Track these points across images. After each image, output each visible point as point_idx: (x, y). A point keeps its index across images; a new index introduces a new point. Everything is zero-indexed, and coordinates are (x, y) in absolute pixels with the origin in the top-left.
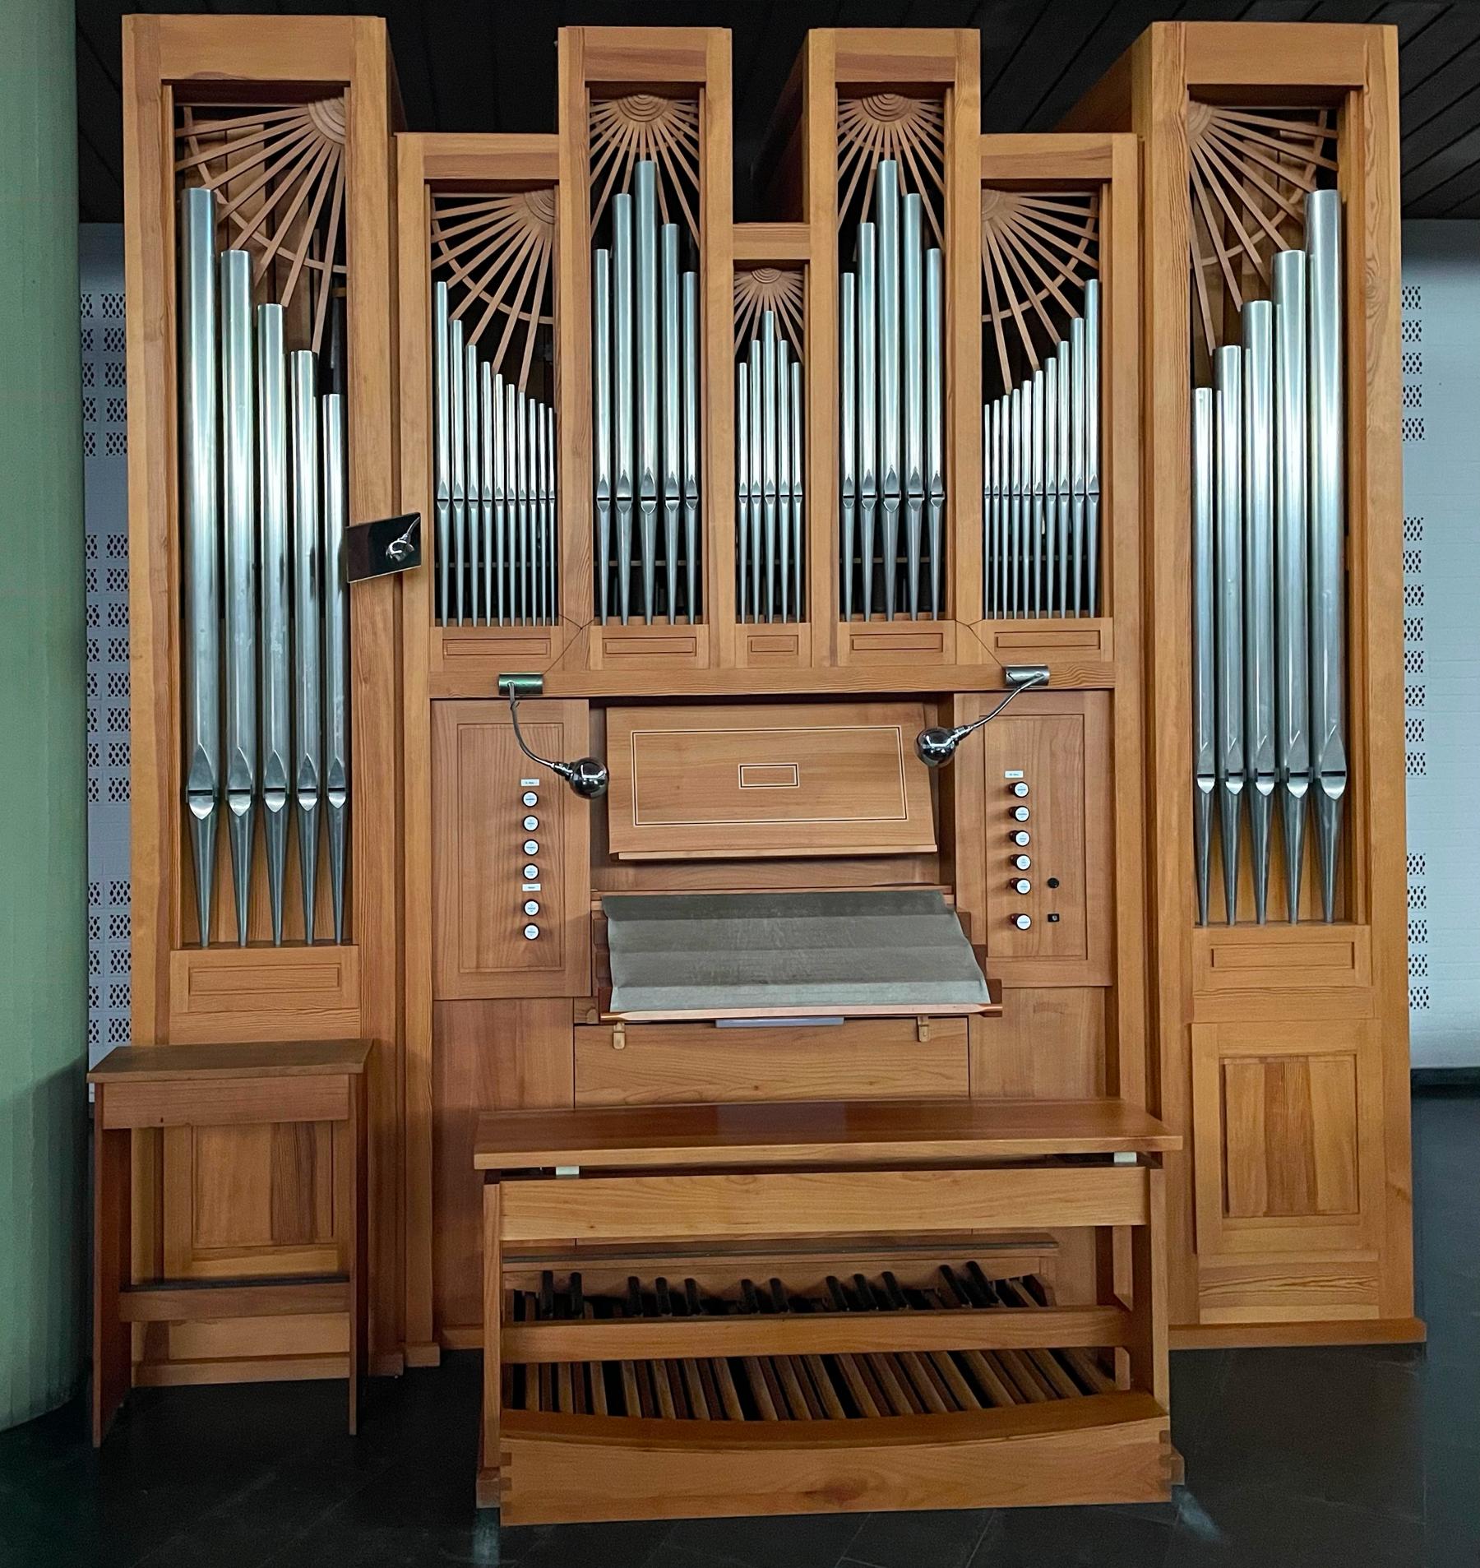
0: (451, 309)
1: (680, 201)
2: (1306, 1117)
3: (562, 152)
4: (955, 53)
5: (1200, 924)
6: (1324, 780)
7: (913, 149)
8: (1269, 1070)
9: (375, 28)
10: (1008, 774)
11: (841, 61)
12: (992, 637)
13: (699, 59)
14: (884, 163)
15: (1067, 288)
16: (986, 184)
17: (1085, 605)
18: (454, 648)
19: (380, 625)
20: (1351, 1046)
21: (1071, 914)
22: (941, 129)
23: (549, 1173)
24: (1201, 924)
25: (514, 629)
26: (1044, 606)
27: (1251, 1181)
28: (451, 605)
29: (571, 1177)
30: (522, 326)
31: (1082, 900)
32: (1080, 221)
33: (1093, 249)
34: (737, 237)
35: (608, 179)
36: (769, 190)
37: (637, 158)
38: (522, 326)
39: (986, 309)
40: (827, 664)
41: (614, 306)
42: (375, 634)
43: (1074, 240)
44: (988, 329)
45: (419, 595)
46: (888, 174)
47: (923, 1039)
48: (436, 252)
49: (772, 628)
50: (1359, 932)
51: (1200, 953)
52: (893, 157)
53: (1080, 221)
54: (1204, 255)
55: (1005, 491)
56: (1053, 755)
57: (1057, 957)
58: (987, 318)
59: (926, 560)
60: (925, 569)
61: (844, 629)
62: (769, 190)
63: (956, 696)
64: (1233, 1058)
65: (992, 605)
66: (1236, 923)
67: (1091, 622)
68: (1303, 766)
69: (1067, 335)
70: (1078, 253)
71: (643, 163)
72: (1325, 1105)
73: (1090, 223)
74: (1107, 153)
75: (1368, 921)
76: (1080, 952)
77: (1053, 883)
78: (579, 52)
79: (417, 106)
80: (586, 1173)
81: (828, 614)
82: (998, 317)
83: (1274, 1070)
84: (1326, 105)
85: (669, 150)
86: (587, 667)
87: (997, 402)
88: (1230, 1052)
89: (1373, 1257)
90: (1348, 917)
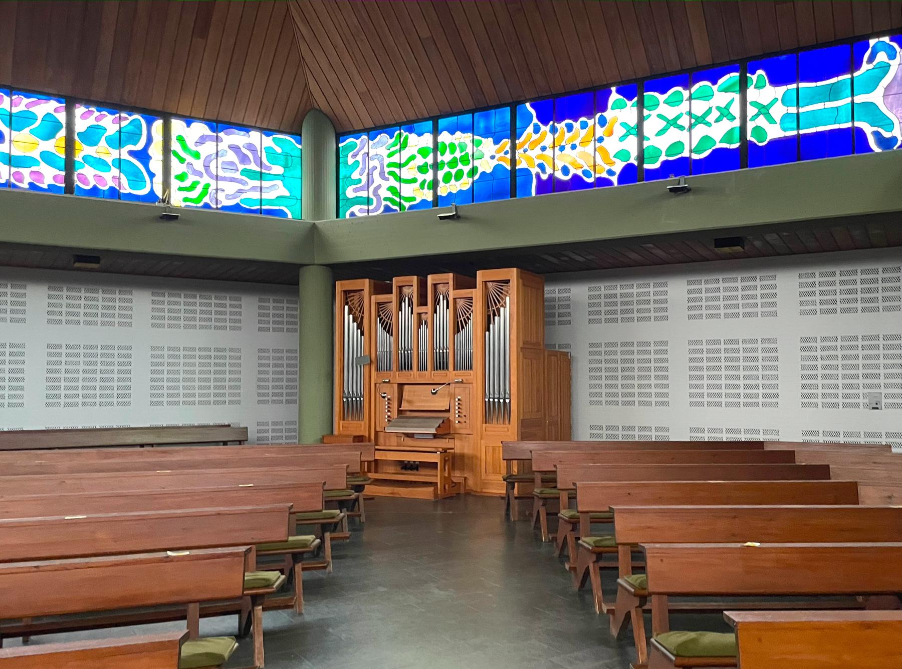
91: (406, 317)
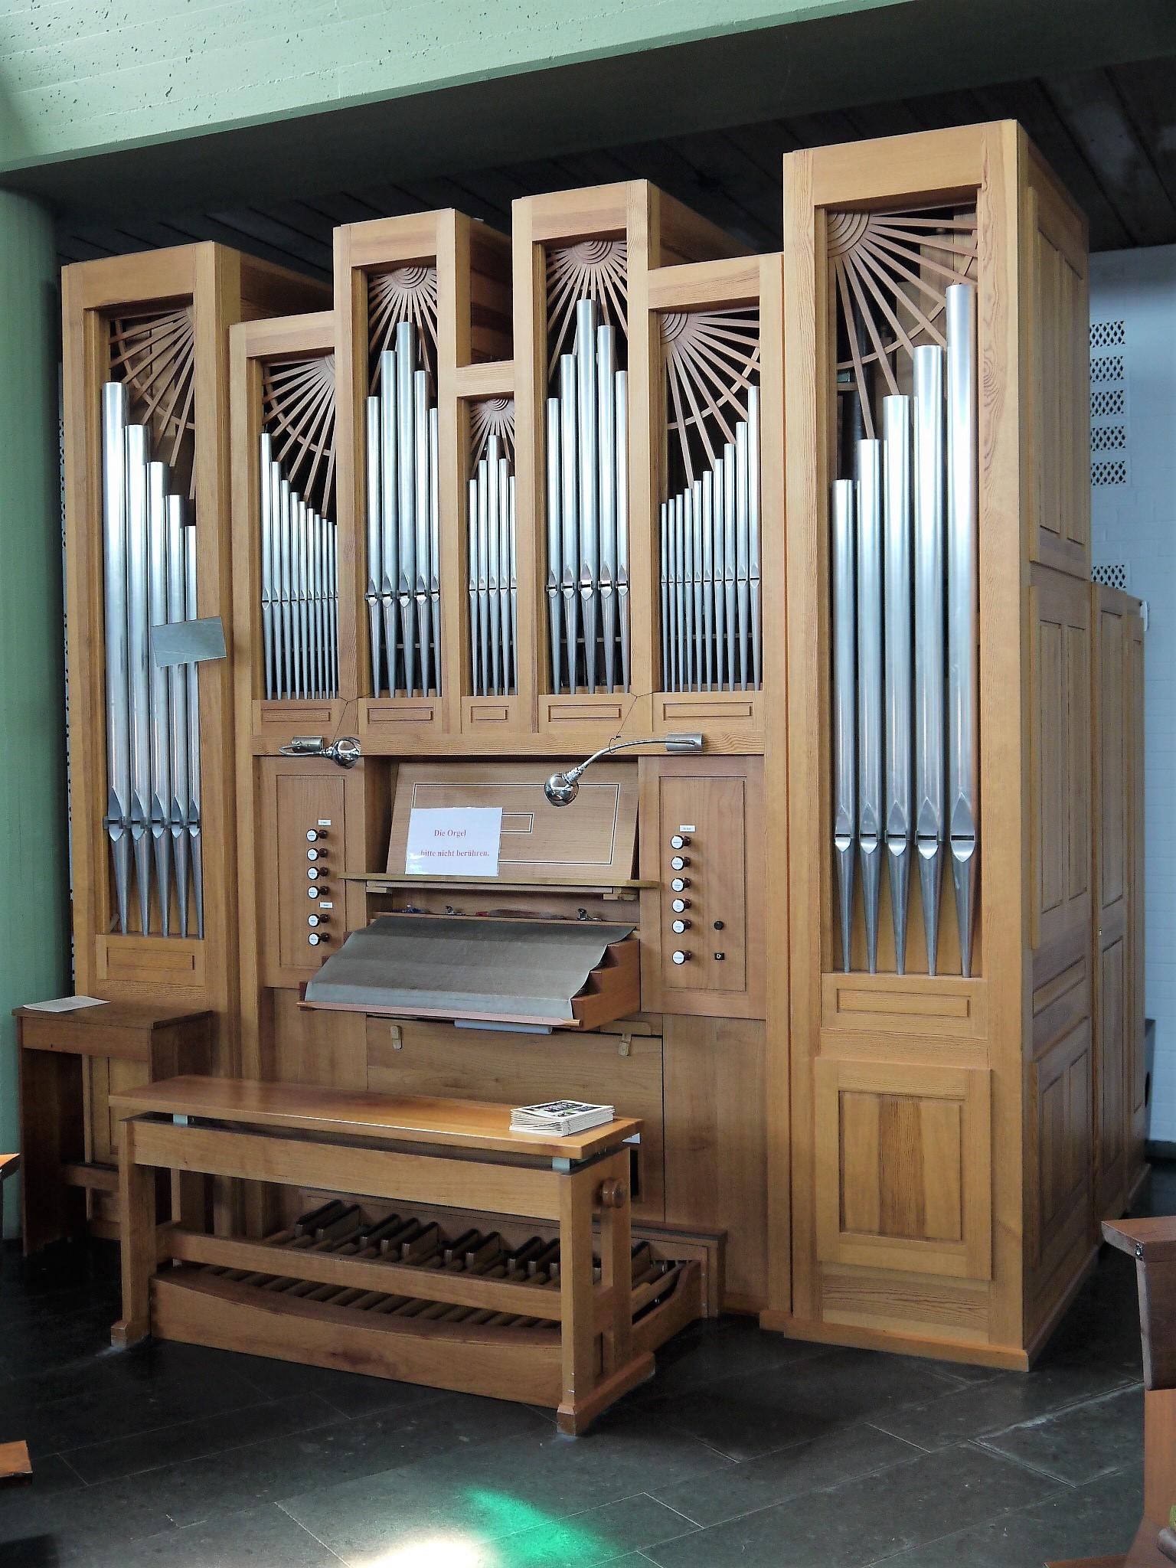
0: (274, 457)
1: (425, 356)
2: (916, 1154)
3: (332, 327)
4: (629, 203)
7: (422, 312)
8: (882, 1106)
9: (1008, 130)
11: (537, 223)
14: (580, 302)
18: (269, 716)
19: (213, 700)
20: (961, 1091)
23: (167, 1118)
25: (306, 702)
26: (714, 680)
27: (865, 1209)
29: (182, 1126)
35: (375, 339)
36: (489, 335)
37: (398, 321)
41: (403, 443)
46: (584, 311)
48: (268, 408)
49: (485, 700)
51: (829, 997)
54: (161, 418)
55: (689, 578)
56: (720, 812)
57: (724, 991)
59: (400, 646)
60: (750, 642)
62: (489, 335)
64: (853, 1092)
71: (401, 324)
72: (936, 1143)
74: (754, 274)
77: (720, 926)
79: (674, 248)
80: (197, 1122)
82: (681, 425)
83: (889, 1106)
84: (955, 204)
85: (606, 289)
87: (679, 497)
88: (853, 1086)
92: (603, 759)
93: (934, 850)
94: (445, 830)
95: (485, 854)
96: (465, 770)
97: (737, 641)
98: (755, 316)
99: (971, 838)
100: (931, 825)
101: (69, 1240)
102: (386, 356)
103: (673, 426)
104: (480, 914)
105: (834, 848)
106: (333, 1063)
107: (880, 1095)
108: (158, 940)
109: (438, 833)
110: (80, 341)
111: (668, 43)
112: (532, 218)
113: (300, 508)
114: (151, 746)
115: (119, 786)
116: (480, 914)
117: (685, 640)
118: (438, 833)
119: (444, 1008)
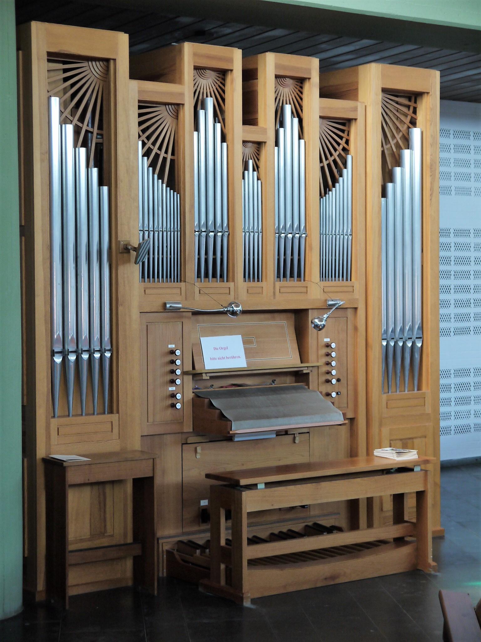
5: (54, 417)
6: (417, 340)
10: (170, 346)
11: (277, 66)
12: (322, 288)
13: (231, 60)
15: (339, 156)
16: (321, 117)
17: (222, 276)
21: (344, 391)
22: (224, 85)
24: (54, 417)
28: (148, 274)
30: (165, 159)
31: (346, 386)
32: (343, 131)
33: (347, 142)
34: (244, 131)
38: (165, 159)
39: (321, 161)
40: (272, 298)
42: (124, 286)
43: (341, 138)
44: (322, 168)
45: (136, 270)
47: (297, 441)
50: (114, 417)
52: (211, 97)
53: (343, 131)
58: (322, 165)
61: (278, 284)
63: (310, 311)
65: (323, 276)
66: (73, 416)
67: (225, 284)
68: (86, 348)
69: (341, 175)
70: (343, 142)
73: (346, 133)
75: (118, 412)
76: (346, 405)
78: (190, 52)
81: (273, 279)
84: (414, 96)
86: (194, 299)
89: (223, 543)
90: (111, 412)
91: (205, 146)
92: (244, 312)
93: (61, 359)
94: (218, 347)
95: (239, 357)
96: (219, 317)
97: (292, 260)
98: (139, 106)
99: (421, 338)
100: (71, 347)
101: (52, 601)
102: (202, 113)
103: (173, 157)
104: (222, 387)
105: (53, 361)
106: (164, 472)
107: (401, 440)
108: (103, 416)
109: (215, 349)
110: (40, 68)
111: (343, 11)
112: (270, 63)
113: (158, 183)
114: (74, 306)
115: (58, 332)
116: (222, 387)
117: (167, 258)
118: (215, 349)
119: (316, 422)
